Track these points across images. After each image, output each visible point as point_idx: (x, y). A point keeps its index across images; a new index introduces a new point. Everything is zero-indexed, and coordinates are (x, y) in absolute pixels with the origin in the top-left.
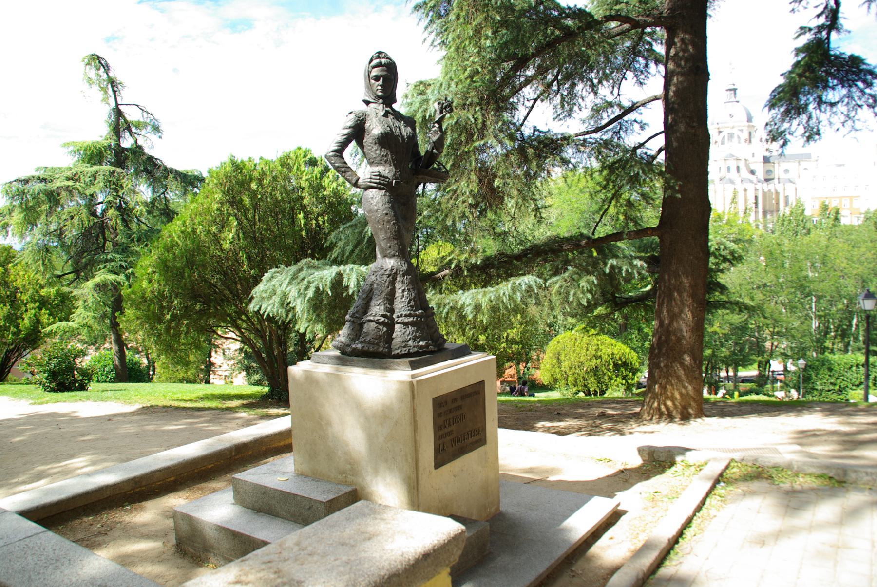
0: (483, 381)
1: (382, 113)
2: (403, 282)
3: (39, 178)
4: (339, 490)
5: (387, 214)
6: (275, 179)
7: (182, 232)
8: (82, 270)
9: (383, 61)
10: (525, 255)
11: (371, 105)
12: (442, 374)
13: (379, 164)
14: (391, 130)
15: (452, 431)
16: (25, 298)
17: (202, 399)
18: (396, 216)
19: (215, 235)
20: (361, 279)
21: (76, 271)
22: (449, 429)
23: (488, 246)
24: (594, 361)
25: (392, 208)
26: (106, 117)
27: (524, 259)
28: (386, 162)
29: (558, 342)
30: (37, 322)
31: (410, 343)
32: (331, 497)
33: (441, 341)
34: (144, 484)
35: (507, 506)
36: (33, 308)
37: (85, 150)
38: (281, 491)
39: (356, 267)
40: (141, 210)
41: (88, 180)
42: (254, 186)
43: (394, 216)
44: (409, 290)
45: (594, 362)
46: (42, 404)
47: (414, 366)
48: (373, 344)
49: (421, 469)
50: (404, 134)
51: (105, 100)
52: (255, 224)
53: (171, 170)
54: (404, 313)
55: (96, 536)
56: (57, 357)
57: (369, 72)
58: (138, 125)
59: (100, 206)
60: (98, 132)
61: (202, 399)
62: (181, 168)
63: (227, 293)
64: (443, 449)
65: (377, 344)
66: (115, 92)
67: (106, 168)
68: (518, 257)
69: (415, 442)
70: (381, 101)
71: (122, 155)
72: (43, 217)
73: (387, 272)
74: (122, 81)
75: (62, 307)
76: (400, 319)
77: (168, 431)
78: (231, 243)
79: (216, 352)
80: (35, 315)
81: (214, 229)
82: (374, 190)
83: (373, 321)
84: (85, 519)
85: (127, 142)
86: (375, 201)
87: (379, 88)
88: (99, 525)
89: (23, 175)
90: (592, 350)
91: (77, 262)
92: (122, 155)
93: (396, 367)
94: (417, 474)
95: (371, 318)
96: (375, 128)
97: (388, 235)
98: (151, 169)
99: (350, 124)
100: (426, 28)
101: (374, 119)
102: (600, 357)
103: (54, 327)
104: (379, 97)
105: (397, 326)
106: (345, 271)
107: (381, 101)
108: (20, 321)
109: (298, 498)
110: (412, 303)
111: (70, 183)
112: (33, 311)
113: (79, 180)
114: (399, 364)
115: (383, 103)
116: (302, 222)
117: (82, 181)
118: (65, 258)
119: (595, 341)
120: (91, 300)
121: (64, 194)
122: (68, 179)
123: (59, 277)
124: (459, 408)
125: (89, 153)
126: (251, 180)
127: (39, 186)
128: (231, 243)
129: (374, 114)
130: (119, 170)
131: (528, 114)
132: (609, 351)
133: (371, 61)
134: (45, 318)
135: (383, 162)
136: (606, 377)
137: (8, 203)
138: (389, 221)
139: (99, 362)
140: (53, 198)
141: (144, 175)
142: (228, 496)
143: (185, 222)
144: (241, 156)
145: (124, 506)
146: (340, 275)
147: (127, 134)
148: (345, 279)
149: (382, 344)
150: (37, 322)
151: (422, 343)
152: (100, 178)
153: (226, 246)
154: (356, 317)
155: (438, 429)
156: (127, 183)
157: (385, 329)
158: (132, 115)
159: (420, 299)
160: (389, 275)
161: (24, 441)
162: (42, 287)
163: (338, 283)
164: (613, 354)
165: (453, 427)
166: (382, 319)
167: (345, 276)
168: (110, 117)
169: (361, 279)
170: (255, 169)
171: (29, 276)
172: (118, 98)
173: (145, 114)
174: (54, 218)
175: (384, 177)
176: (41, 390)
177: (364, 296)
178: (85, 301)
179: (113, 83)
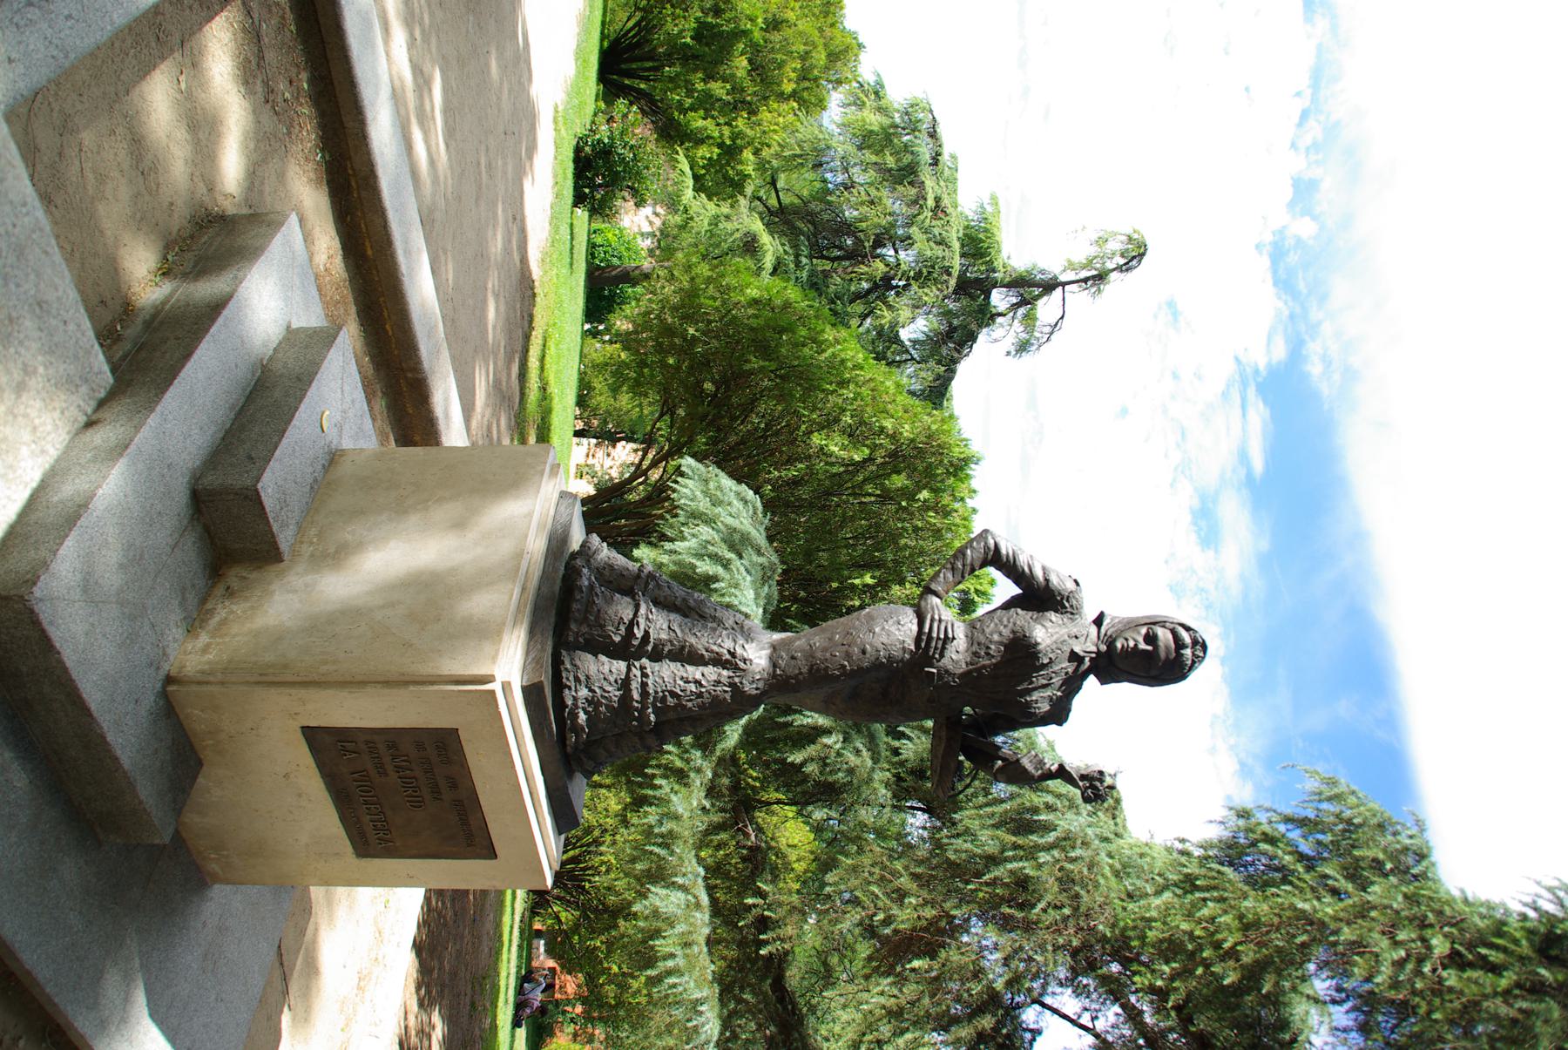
1: (1077, 649)
2: (718, 683)
3: (938, 154)
4: (284, 525)
5: (864, 652)
6: (937, 533)
7: (843, 361)
8: (781, 218)
9: (1188, 652)
11: (1094, 629)
13: (971, 640)
14: (1044, 666)
15: (387, 775)
16: (740, 123)
17: (544, 389)
18: (860, 672)
19: (837, 420)
21: (782, 209)
22: (390, 768)
23: (803, 937)
25: (877, 665)
26: (1042, 265)
28: (975, 654)
30: (699, 140)
32: (269, 503)
33: (589, 765)
34: (364, 194)
35: (221, 902)
36: (722, 135)
37: (986, 230)
38: (296, 409)
40: (883, 317)
41: (936, 231)
42: (924, 495)
43: (860, 669)
44: (700, 695)
46: (555, 121)
47: (532, 694)
48: (587, 611)
49: (302, 693)
50: (1035, 696)
51: (1071, 266)
52: (854, 495)
53: (953, 372)
54: (650, 682)
55: (266, 83)
56: (635, 159)
58: (1029, 319)
59: (892, 252)
60: (1017, 251)
61: (544, 389)
62: (957, 387)
63: (733, 439)
64: (344, 749)
66: (1085, 280)
67: (957, 263)
69: (362, 684)
70: (1103, 648)
71: (977, 292)
72: (874, 158)
73: (739, 651)
74: (1104, 294)
75: (719, 180)
76: (638, 673)
77: (484, 310)
78: (822, 449)
79: (636, 451)
80: (709, 137)
81: (847, 419)
82: (915, 628)
83: (635, 615)
84: (304, 76)
85: (1000, 299)
86: (893, 629)
87: (1132, 644)
88: (287, 95)
89: (942, 130)
91: (796, 211)
92: (977, 292)
94: (292, 684)
95: (643, 610)
96: (1046, 632)
97: (819, 655)
98: (954, 340)
99: (1054, 580)
103: (685, 165)
104: (1111, 643)
105: (622, 665)
107: (1103, 648)
108: (702, 112)
109: (276, 439)
110: (671, 701)
111: (931, 203)
112: (716, 134)
113: (935, 217)
115: (1098, 652)
116: (857, 581)
117: (934, 223)
118: (805, 193)
120: (729, 226)
121: (913, 191)
122: (938, 200)
123: (773, 183)
124: (436, 791)
125: (981, 236)
126: (935, 491)
127: (925, 152)
128: (822, 449)
129: (1074, 631)
130: (953, 282)
131: (1065, 1017)
133: (1188, 629)
134: (703, 152)
137: (896, 106)
138: (848, 656)
139: (628, 249)
140: (906, 174)
141: (944, 328)
142: (311, 317)
143: (862, 368)
144: (979, 476)
145: (322, 150)
147: (1014, 300)
149: (585, 629)
150: (699, 140)
151: (582, 717)
152: (939, 251)
153: (817, 439)
154: (647, 584)
155: (393, 737)
156: (930, 294)
157: (617, 639)
158: (1047, 308)
159: (681, 720)
160: (733, 654)
161: (489, 72)
162: (756, 153)
165: (393, 777)
166: (639, 633)
168: (1042, 272)
170: (955, 499)
171: (775, 131)
172: (1074, 287)
173: (1048, 329)
174: (872, 174)
175: (944, 648)
176: (581, 131)
178: (728, 217)
179: (1100, 277)
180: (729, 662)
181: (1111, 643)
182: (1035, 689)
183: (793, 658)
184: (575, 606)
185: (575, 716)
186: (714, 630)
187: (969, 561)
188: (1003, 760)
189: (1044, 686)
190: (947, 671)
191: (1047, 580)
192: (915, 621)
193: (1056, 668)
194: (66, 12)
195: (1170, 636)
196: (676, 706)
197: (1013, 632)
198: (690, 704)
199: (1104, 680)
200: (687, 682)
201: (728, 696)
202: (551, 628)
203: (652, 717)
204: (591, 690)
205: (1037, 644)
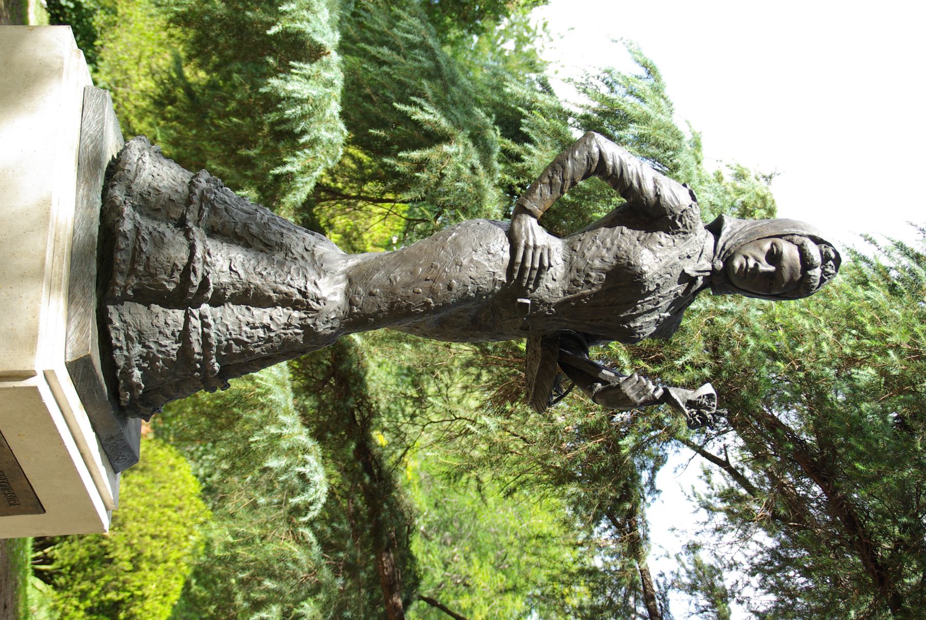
0: (45, 511)
1: (690, 270)
2: (288, 325)
5: (450, 288)
10: (368, 469)
11: (711, 238)
12: (62, 442)
13: (570, 265)
14: (649, 293)
20: (308, 107)
24: (127, 555)
25: (465, 299)
27: (359, 465)
28: (574, 281)
29: (173, 467)
31: (138, 349)
39: (337, 92)
43: (446, 305)
44: (270, 340)
45: (123, 555)
47: (79, 370)
48: (134, 261)
57: (789, 237)
65: (133, 271)
68: (365, 449)
70: (719, 264)
73: (311, 289)
82: (507, 256)
87: (751, 263)
90: (154, 548)
93: (74, 322)
95: (199, 254)
96: (655, 258)
97: (400, 291)
100: (900, 246)
101: (675, 253)
102: (136, 569)
105: (179, 314)
106: (327, 66)
110: (236, 349)
114: (81, 328)
115: (713, 271)
119: (174, 555)
129: (687, 250)
132: (151, 589)
133: (817, 241)
135: (574, 275)
136: (85, 586)
138: (432, 292)
146: (315, 53)
148: (307, 68)
151: (137, 373)
157: (171, 287)
160: (304, 294)
163: (299, 48)
164: (143, 598)
166: (196, 281)
167: (315, 67)
169: (308, 107)
175: (538, 278)
177: (254, 229)
180: (300, 302)
183: (371, 294)
184: (119, 256)
185: (128, 375)
186: (281, 264)
187: (569, 176)
188: (604, 382)
190: (542, 301)
191: (658, 196)
192: (507, 247)
193: (663, 292)
195: (797, 254)
196: (242, 353)
197: (617, 257)
198: (258, 350)
200: (254, 327)
201: (300, 339)
202: (93, 285)
203: (217, 367)
204: (144, 346)
205: (643, 273)
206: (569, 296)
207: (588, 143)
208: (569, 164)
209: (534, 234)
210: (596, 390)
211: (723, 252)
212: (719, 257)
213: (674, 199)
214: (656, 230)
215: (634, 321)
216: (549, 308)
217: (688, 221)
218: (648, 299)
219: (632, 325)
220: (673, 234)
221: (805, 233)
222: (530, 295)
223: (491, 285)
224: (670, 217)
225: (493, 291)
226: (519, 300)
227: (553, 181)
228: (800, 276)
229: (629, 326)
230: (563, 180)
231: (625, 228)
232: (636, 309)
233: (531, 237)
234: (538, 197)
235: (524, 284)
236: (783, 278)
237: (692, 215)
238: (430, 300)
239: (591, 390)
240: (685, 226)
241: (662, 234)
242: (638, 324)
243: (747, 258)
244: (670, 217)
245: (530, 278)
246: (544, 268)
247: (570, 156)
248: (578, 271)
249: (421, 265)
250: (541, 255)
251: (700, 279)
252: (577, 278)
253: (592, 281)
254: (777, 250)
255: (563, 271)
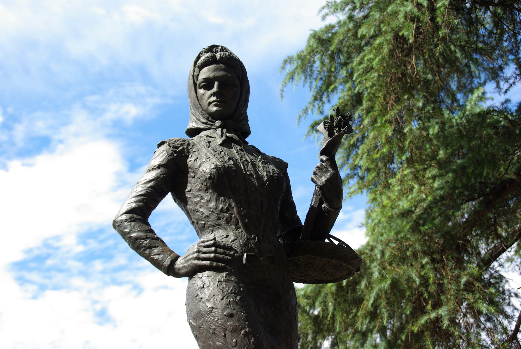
1: (220, 141)
5: (231, 316)
13: (216, 226)
14: (236, 164)
25: (243, 304)
28: (228, 222)
43: (247, 319)
70: (218, 123)
82: (207, 273)
96: (205, 161)
107: (218, 123)
115: (222, 127)
133: (199, 58)
135: (222, 222)
138: (235, 330)
175: (224, 247)
181: (212, 117)
182: (257, 173)
189: (254, 166)
190: (245, 244)
191: (159, 166)
192: (200, 275)
193: (237, 156)
194: (385, 235)
195: (205, 69)
197: (206, 190)
199: (247, 133)
205: (216, 167)
206: (240, 224)
207: (119, 224)
208: (134, 235)
209: (189, 255)
210: (327, 207)
211: (209, 123)
212: (212, 125)
213: (161, 155)
214: (187, 165)
215: (263, 177)
216: (251, 239)
217: (178, 142)
218: (242, 167)
219: (266, 179)
220: (189, 152)
221: (192, 69)
222: (240, 253)
223: (229, 283)
224: (175, 155)
225: (235, 282)
226: (244, 262)
227: (148, 245)
228: (221, 65)
229: (267, 181)
230: (147, 238)
231: (187, 190)
232: (251, 175)
233: (191, 257)
234: (161, 256)
235: (229, 258)
236: (223, 76)
237: (174, 141)
238: (242, 332)
239: (328, 211)
240: (182, 145)
241: (188, 160)
242: (265, 174)
243: (210, 103)
244: (175, 155)
245: (224, 254)
246: (214, 243)
247: (129, 236)
248: (219, 219)
249: (214, 343)
250: (205, 247)
251: (228, 135)
252: (225, 219)
253: (226, 207)
254: (203, 82)
255: (220, 231)
